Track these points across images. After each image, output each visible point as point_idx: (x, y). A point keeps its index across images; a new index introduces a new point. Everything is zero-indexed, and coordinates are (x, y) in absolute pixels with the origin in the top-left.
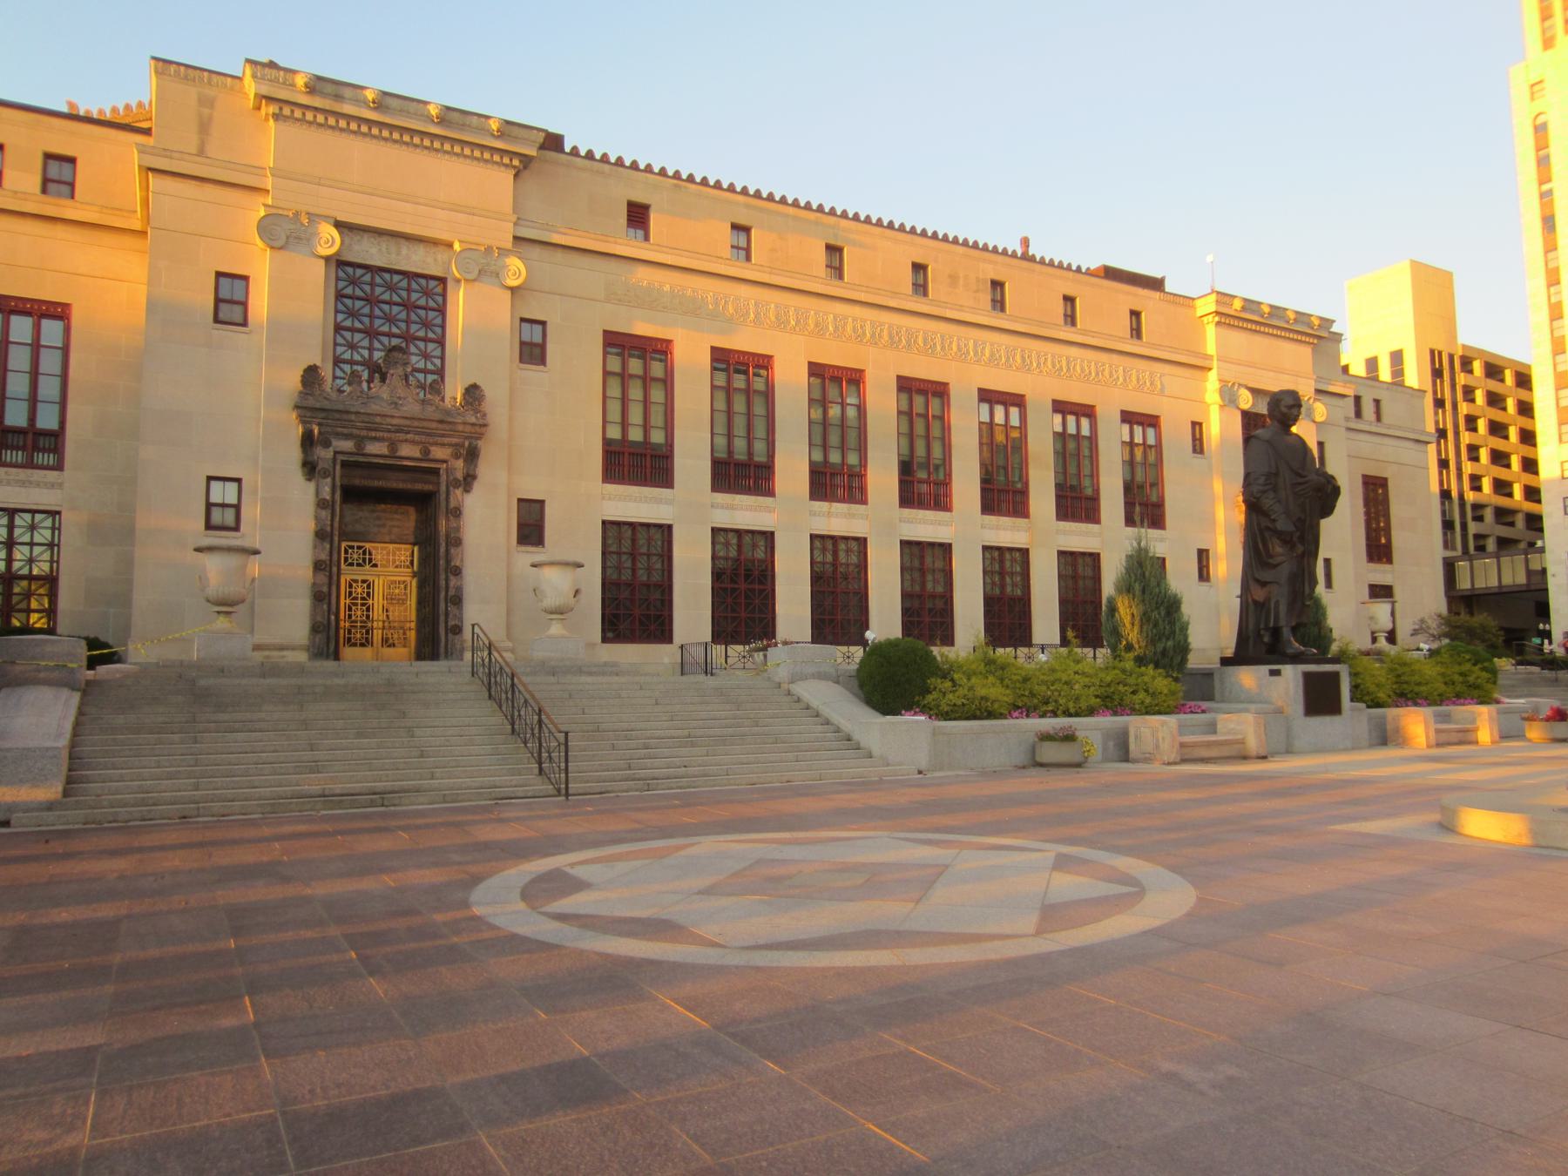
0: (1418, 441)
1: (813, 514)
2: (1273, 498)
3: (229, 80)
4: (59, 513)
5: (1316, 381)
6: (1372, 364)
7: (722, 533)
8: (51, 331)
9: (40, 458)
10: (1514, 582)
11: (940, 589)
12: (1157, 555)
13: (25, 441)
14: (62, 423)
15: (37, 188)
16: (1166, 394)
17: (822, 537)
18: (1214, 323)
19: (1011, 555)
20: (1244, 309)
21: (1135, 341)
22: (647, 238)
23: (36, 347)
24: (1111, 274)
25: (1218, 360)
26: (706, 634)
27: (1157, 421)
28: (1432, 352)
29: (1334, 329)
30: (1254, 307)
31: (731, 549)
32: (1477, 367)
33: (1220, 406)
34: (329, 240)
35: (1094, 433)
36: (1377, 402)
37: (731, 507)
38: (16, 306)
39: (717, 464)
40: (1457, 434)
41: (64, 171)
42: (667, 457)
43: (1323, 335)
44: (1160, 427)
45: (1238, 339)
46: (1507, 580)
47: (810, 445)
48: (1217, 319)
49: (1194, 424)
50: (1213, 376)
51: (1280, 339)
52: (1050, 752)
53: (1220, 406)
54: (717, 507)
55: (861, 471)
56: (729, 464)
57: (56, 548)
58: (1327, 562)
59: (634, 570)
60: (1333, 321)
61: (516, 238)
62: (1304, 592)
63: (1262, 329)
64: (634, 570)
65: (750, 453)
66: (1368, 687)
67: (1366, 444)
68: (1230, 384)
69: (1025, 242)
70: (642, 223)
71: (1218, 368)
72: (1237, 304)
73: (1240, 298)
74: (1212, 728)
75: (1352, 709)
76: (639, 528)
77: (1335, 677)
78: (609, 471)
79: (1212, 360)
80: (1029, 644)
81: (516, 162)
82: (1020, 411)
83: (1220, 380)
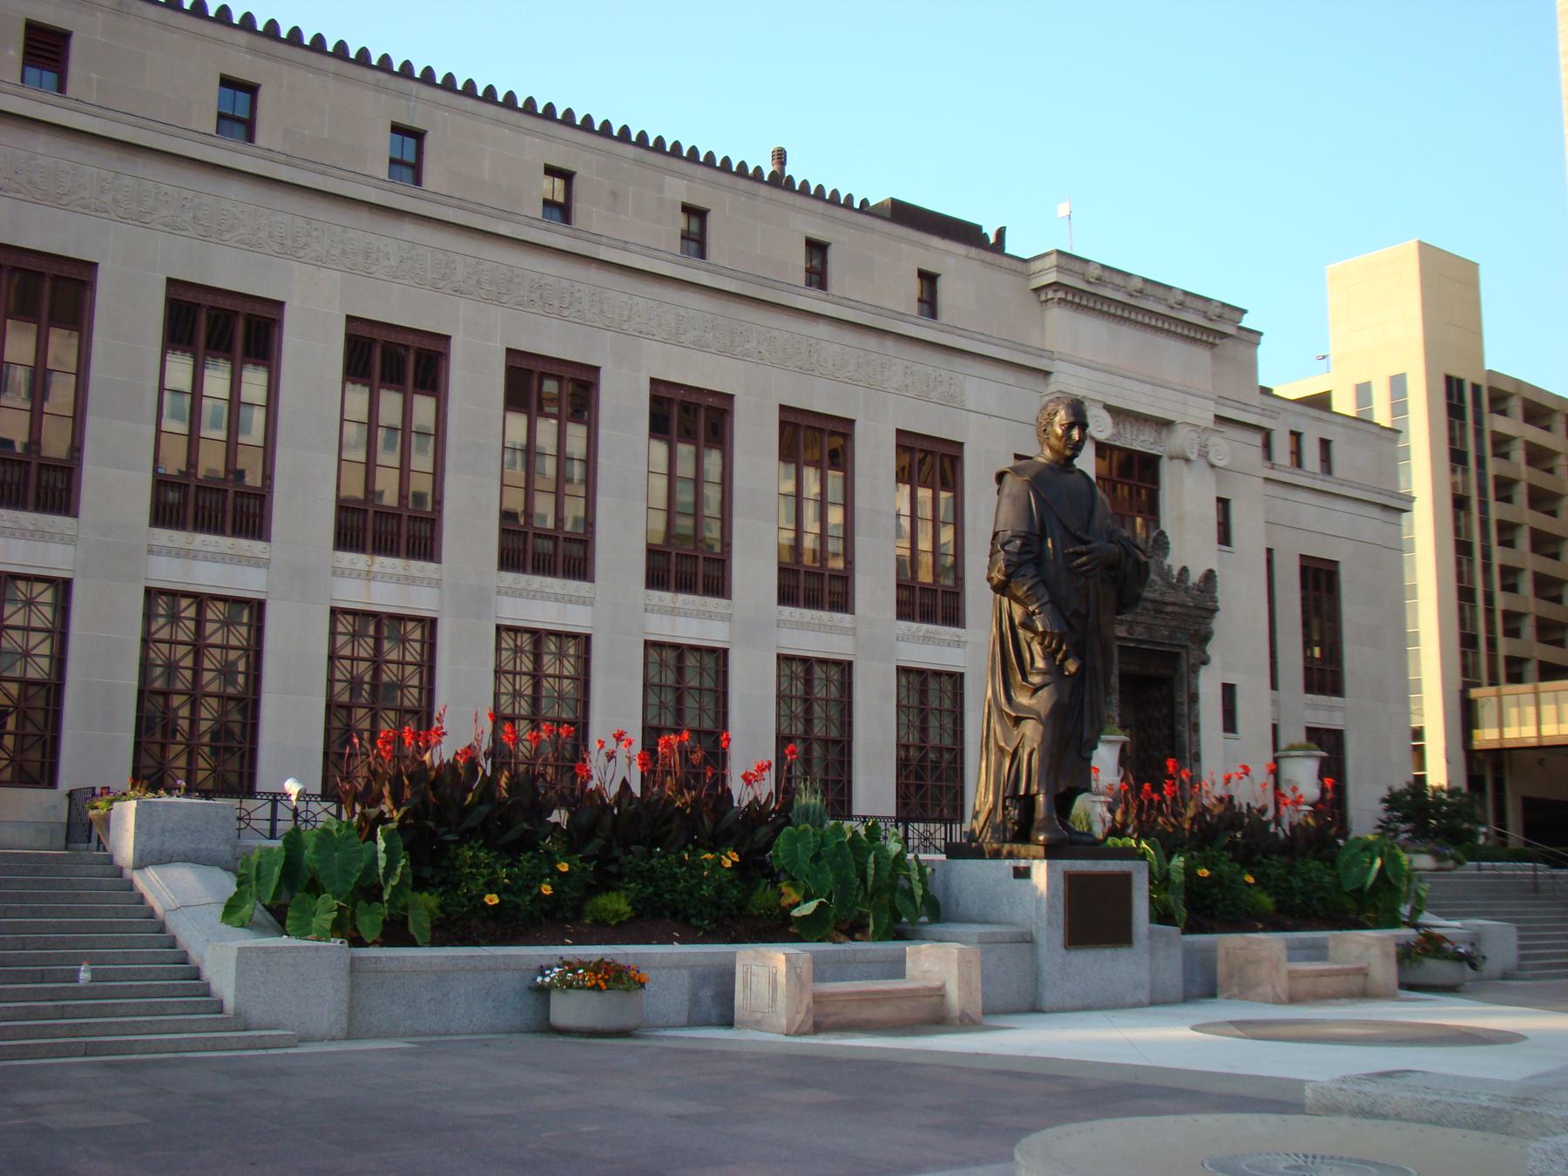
0: (1385, 507)
1: (337, 572)
2: (1035, 576)
6: (1363, 392)
7: (553, 638)
10: (1539, 735)
11: (947, 741)
19: (790, 668)
21: (925, 321)
22: (61, 88)
24: (903, 214)
26: (888, 807)
28: (1449, 379)
29: (1246, 322)
31: (565, 662)
32: (1515, 406)
36: (1325, 444)
39: (161, 483)
40: (1483, 505)
43: (1230, 332)
46: (1524, 735)
47: (502, 485)
52: (567, 1009)
54: (159, 553)
58: (1229, 691)
60: (1244, 312)
61: (1217, 417)
62: (1082, 735)
63: (1133, 316)
65: (559, 519)
67: (1308, 510)
69: (780, 156)
70: (57, 61)
74: (896, 968)
77: (1125, 879)
80: (850, 817)
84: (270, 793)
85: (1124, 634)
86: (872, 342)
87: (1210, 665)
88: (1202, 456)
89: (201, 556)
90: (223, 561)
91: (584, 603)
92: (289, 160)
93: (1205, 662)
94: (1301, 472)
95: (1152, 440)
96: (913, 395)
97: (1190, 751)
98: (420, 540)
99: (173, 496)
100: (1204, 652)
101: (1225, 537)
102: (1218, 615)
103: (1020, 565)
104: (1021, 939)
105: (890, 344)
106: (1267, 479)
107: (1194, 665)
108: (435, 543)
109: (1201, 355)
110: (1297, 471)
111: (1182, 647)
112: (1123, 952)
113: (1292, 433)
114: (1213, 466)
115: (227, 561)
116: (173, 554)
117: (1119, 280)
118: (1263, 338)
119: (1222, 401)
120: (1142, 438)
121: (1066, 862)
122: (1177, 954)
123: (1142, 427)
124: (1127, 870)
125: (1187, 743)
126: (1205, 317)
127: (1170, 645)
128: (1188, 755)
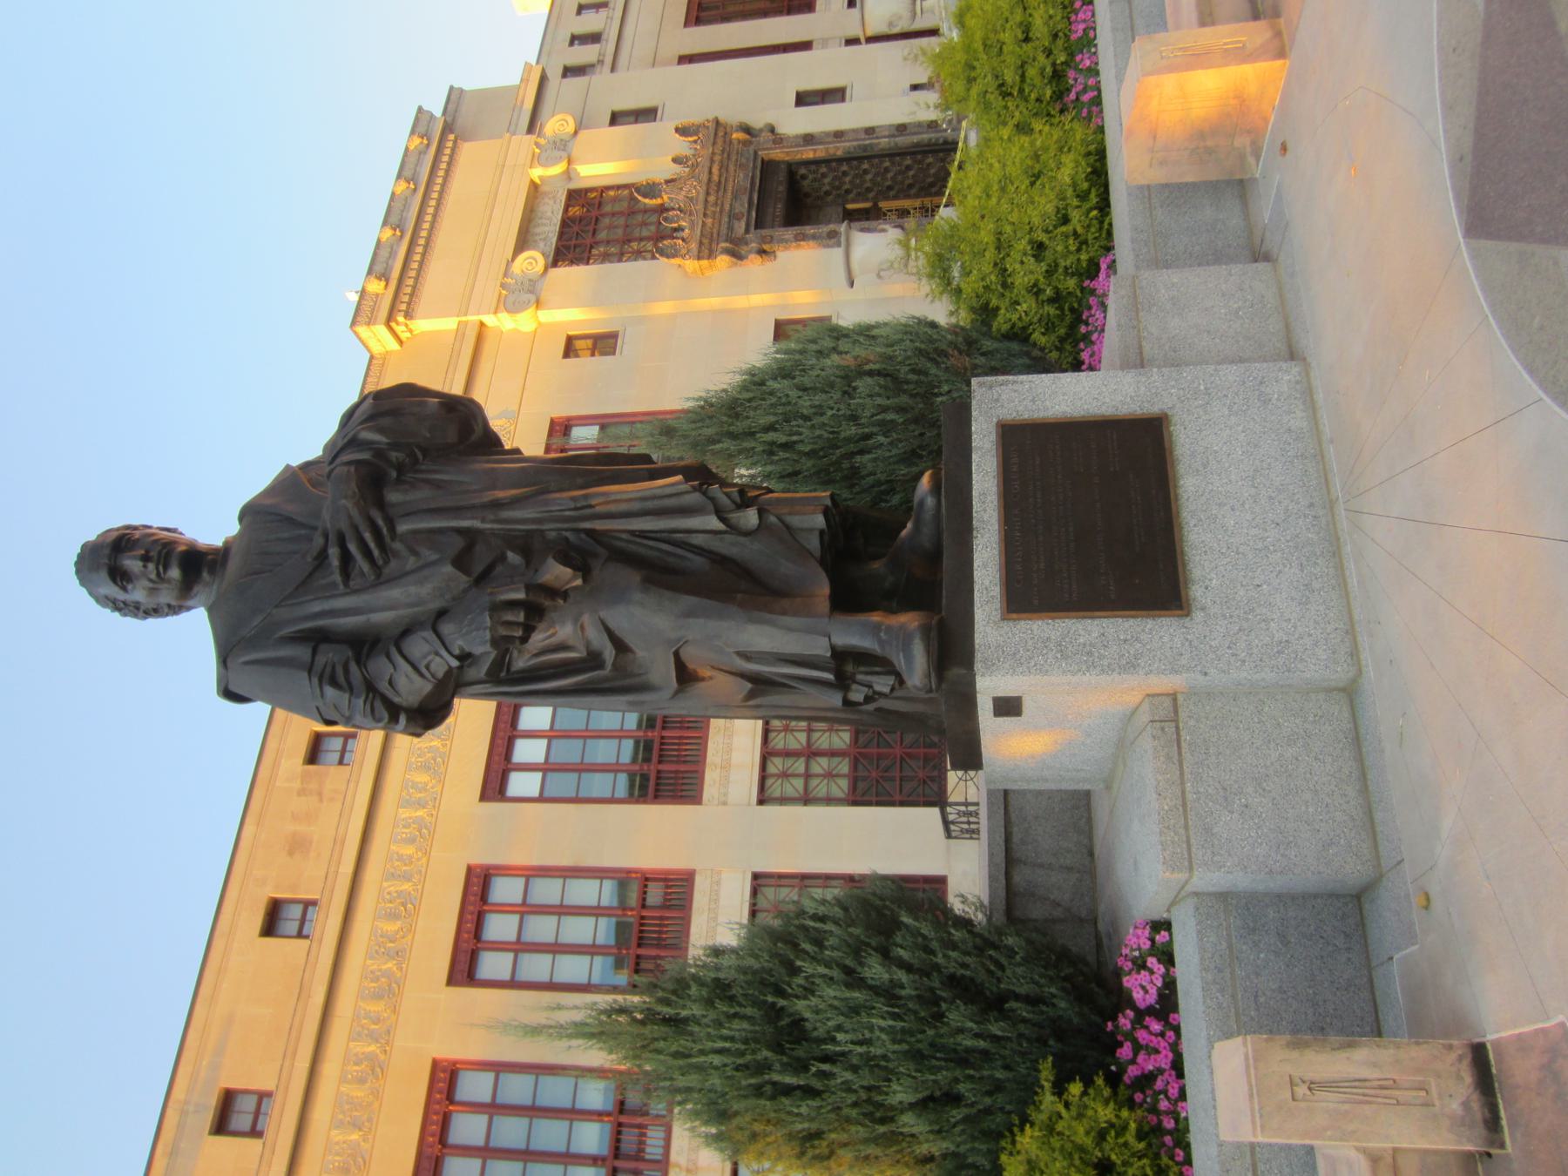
3: (369, 380)
5: (514, 134)
12: (745, 921)
16: (515, 408)
18: (408, 322)
20: (384, 276)
25: (466, 315)
27: (560, 424)
29: (437, 108)
30: (398, 205)
33: (537, 307)
34: (532, 261)
35: (520, 872)
37: (726, 767)
38: (468, 932)
44: (569, 419)
45: (440, 274)
48: (401, 319)
49: (570, 350)
50: (489, 320)
51: (433, 237)
53: (537, 307)
55: (636, 878)
58: (802, 99)
59: (832, 753)
60: (420, 109)
63: (424, 234)
64: (832, 753)
66: (1044, 216)
68: (537, 151)
71: (479, 313)
72: (376, 287)
73: (381, 232)
75: (1138, 362)
77: (1013, 436)
78: (688, 758)
79: (466, 323)
81: (452, 137)
82: (577, 425)
83: (496, 312)
85: (743, 224)
87: (774, 123)
88: (565, 145)
91: (718, 883)
93: (772, 130)
94: (607, 31)
95: (551, 202)
97: (864, 139)
100: (761, 130)
101: (646, 115)
102: (722, 118)
103: (371, 688)
104: (1170, 728)
106: (613, 69)
107: (774, 142)
109: (468, 151)
110: (604, 37)
111: (756, 153)
112: (1185, 442)
113: (571, 44)
114: (576, 133)
117: (384, 253)
118: (456, 86)
119: (513, 127)
120: (549, 214)
121: (980, 615)
122: (1166, 283)
123: (539, 214)
124: (993, 437)
125: (855, 143)
126: (425, 153)
127: (755, 167)
128: (867, 142)
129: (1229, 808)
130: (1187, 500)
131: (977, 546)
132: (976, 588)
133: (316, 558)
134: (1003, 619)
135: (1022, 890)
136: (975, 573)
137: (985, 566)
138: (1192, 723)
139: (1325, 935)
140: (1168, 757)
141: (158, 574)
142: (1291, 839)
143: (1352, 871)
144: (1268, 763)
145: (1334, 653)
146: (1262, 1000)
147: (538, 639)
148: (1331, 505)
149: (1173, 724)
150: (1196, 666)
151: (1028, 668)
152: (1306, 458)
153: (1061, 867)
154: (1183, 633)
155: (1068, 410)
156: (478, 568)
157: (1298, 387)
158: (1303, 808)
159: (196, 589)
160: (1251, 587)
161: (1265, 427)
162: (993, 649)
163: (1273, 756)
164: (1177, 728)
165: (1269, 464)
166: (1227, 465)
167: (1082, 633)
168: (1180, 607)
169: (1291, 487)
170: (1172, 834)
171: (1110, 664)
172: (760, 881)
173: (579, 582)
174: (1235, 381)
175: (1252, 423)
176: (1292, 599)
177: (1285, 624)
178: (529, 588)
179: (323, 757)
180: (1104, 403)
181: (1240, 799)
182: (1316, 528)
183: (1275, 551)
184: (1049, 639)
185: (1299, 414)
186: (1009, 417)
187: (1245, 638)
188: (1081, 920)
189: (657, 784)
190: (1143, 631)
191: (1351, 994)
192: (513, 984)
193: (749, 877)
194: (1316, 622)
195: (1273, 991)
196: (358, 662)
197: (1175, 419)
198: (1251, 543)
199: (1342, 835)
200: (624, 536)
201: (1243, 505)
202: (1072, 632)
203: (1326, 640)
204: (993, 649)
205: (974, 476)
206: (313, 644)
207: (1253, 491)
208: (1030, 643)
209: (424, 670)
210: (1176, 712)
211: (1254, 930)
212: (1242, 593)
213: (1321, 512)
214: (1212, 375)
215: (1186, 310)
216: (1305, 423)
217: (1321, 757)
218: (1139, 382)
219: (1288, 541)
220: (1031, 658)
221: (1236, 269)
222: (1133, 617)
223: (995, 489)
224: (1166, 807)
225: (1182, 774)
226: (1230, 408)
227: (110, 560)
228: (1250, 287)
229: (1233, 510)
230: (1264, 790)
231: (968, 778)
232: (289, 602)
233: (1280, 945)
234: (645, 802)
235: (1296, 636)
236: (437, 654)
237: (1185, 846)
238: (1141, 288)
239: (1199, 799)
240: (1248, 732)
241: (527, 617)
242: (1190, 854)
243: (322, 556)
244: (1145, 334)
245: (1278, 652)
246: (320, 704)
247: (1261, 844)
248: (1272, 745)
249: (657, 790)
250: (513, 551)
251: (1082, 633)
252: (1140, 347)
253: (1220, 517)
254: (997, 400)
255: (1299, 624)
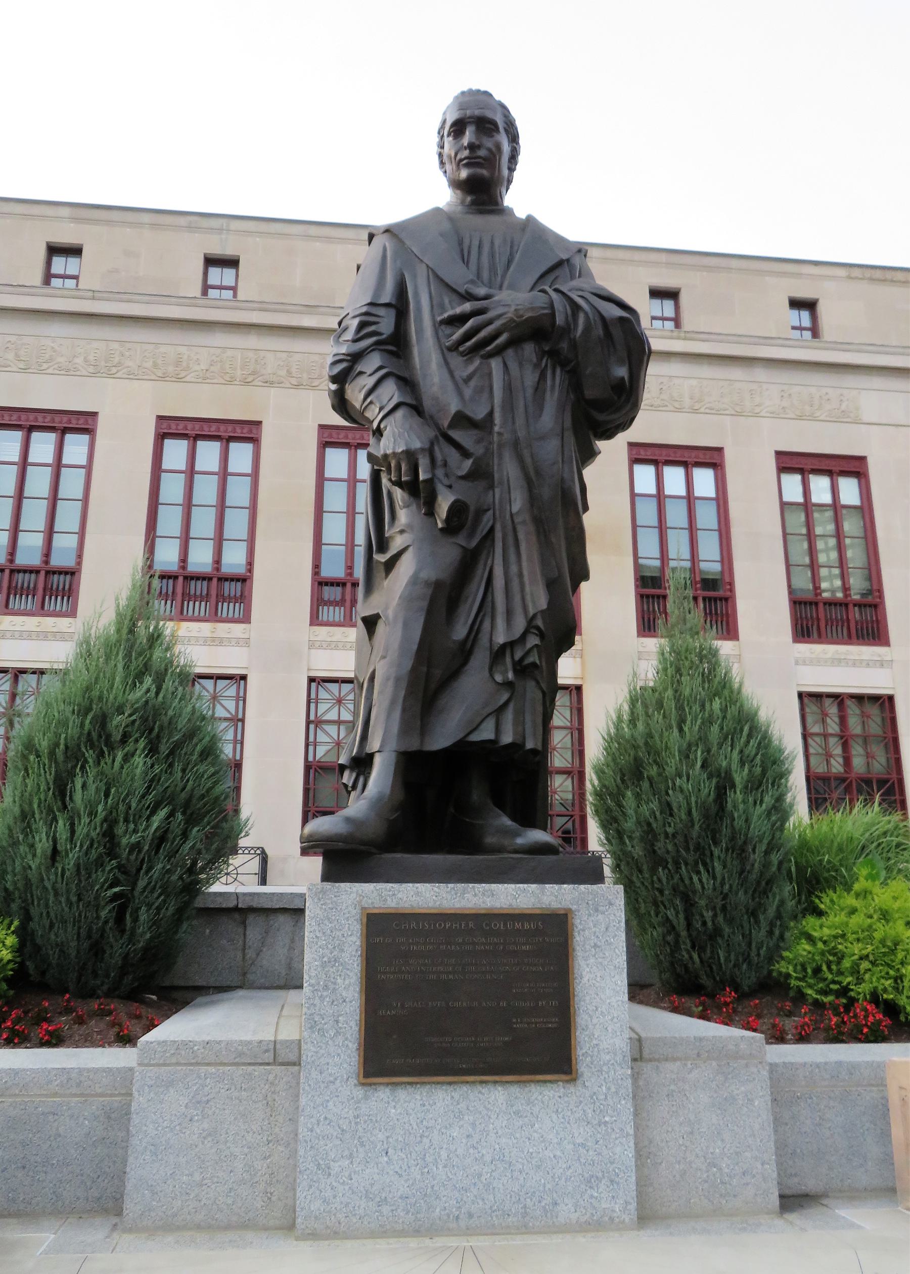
4: (244, 678)
8: (240, 454)
9: (225, 609)
13: (343, 594)
14: (250, 564)
15: (198, 293)
16: (866, 420)
17: (817, 697)
23: (224, 474)
41: (227, 276)
42: (726, 599)
56: (816, 604)
57: (240, 724)
65: (846, 589)
76: (848, 702)
84: (258, 848)
86: (736, 373)
89: (8, 635)
90: (29, 638)
92: (263, 306)
96: (793, 416)
98: (867, 624)
99: (809, 611)
104: (269, 1057)
105: (761, 374)
108: (880, 625)
115: (34, 637)
116: (17, 636)
121: (368, 888)
124: (555, 905)
129: (190, 1105)
130: (480, 1092)
131: (438, 887)
132: (395, 886)
133: (467, 292)
134: (363, 909)
135: (272, 922)
136: (411, 885)
137: (418, 894)
138: (271, 1077)
139: (99, 1180)
140: (241, 1054)
141: (461, 160)
142: (160, 1157)
143: (130, 1207)
144: (228, 1145)
145: (316, 1217)
146: (51, 1117)
147: (399, 494)
148: (470, 1232)
149: (271, 1061)
150: (309, 1085)
151: (315, 931)
152: (523, 1217)
153: (291, 959)
154: (342, 1077)
155: (585, 980)
156: (455, 435)
157: (607, 1219)
158: (187, 1172)
159: (459, 192)
160: (386, 1146)
161: (560, 1178)
162: (335, 899)
163: (236, 1149)
164: (268, 1064)
165: (517, 1179)
166: (518, 1135)
167: (347, 982)
168: (367, 1075)
169: (491, 1197)
170: (172, 1052)
171: (315, 1005)
172: (574, 692)
173: (440, 525)
174: (615, 1154)
175: (564, 1166)
176: (372, 1185)
177: (347, 1174)
178: (430, 482)
179: (657, 302)
180: (591, 1017)
181: (197, 1115)
182: (445, 1218)
183: (422, 1173)
184: (342, 950)
185: (574, 1217)
186: (577, 921)
187: (335, 1134)
188: (244, 974)
189: (653, 597)
190: (347, 1039)
191: (50, 1196)
192: (321, 479)
193: (578, 682)
194: (347, 1205)
195: (57, 1129)
196: (377, 343)
197: (571, 1088)
198: (431, 1151)
199: (160, 1204)
200: (489, 562)
201: (474, 1147)
202: (348, 972)
203: (330, 1212)
204: (335, 899)
205: (513, 886)
206: (394, 302)
207: (488, 1158)
208: (339, 933)
209: (369, 400)
210: (282, 1064)
211: (109, 1118)
212: (381, 1136)
213: (462, 1224)
214: (622, 1130)
215: (719, 1112)
216: (563, 1221)
217: (232, 1194)
218: (615, 1054)
219: (433, 1187)
220: (324, 933)
221: (771, 1171)
222: (360, 1029)
223: (498, 905)
224: (196, 1048)
225: (225, 1064)
226: (583, 1145)
227: (469, 118)
228: (747, 1184)
229: (468, 1136)
230: (204, 1138)
231: (235, 872)
232: (431, 276)
233: (94, 1139)
234: (637, 586)
235: (334, 1184)
236: (381, 409)
237: (161, 1062)
238: (747, 1066)
239: (199, 1077)
240: (259, 1128)
241: (406, 482)
242: (153, 1065)
243: (469, 297)
244: (689, 1066)
245: (319, 1164)
246: (349, 317)
247: (157, 1129)
248: (246, 1150)
249: (648, 596)
250: (473, 463)
251: (347, 982)
252: (675, 1060)
253: (461, 1123)
254: (597, 910)
255: (347, 1187)
